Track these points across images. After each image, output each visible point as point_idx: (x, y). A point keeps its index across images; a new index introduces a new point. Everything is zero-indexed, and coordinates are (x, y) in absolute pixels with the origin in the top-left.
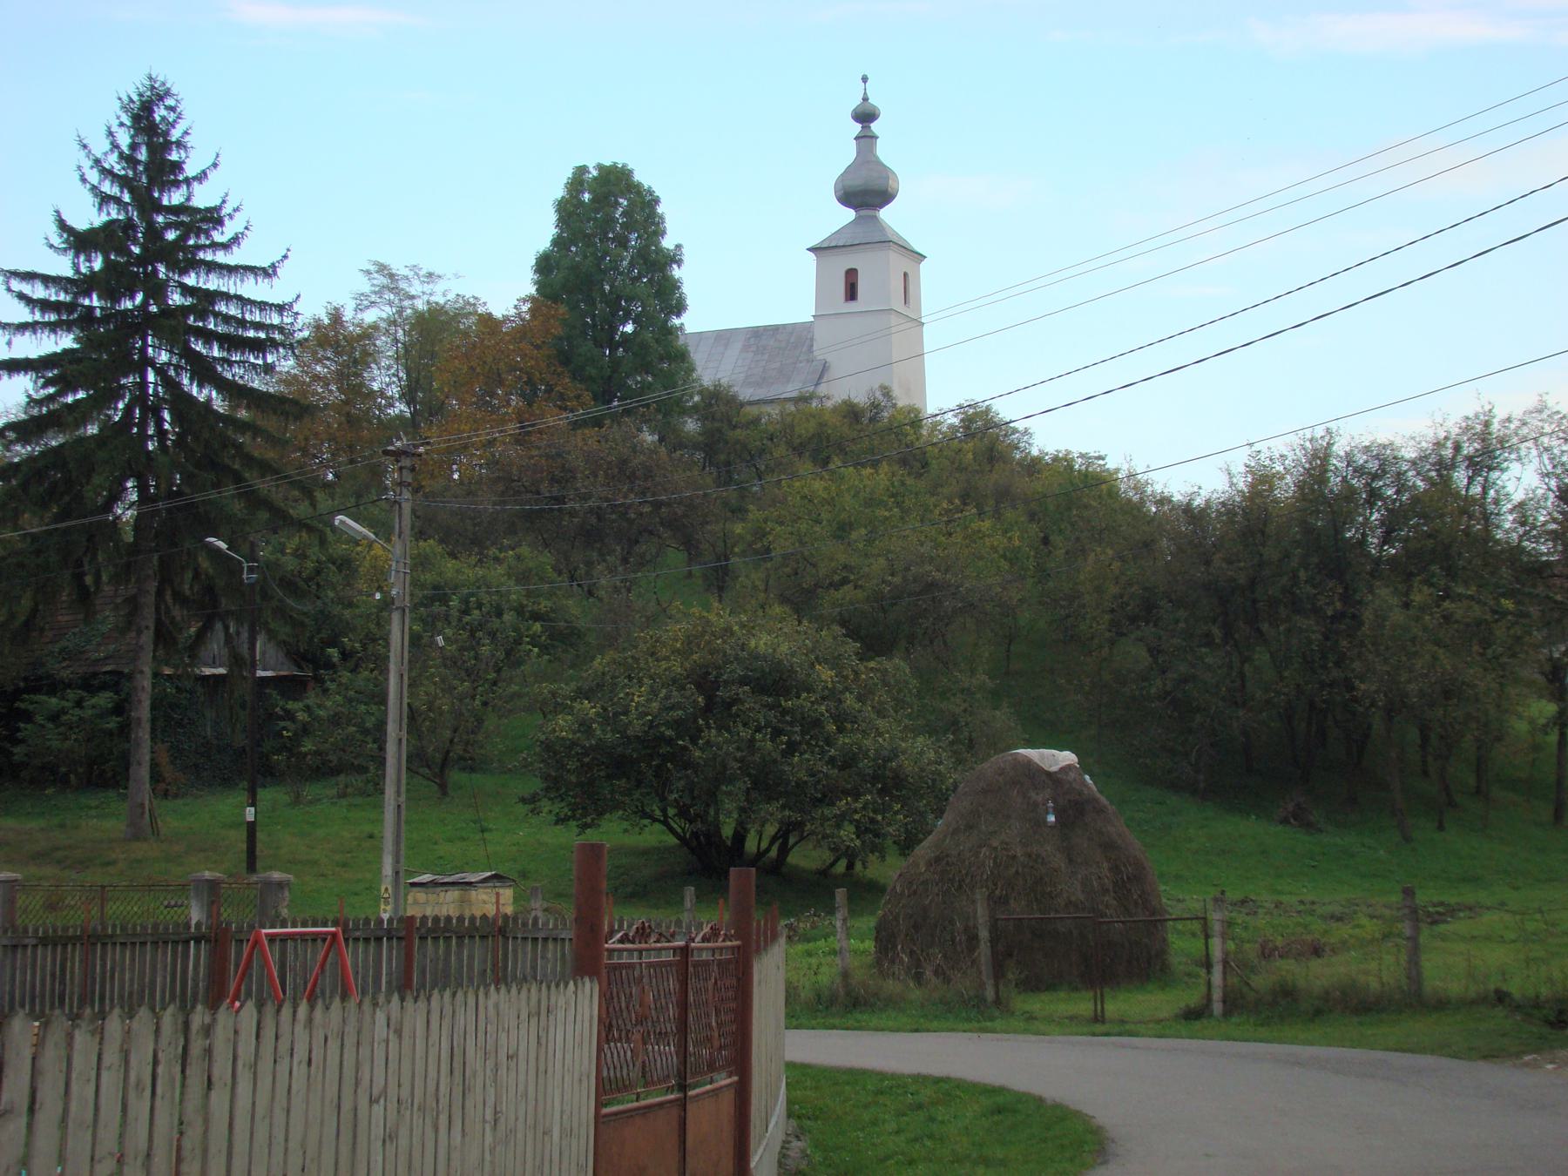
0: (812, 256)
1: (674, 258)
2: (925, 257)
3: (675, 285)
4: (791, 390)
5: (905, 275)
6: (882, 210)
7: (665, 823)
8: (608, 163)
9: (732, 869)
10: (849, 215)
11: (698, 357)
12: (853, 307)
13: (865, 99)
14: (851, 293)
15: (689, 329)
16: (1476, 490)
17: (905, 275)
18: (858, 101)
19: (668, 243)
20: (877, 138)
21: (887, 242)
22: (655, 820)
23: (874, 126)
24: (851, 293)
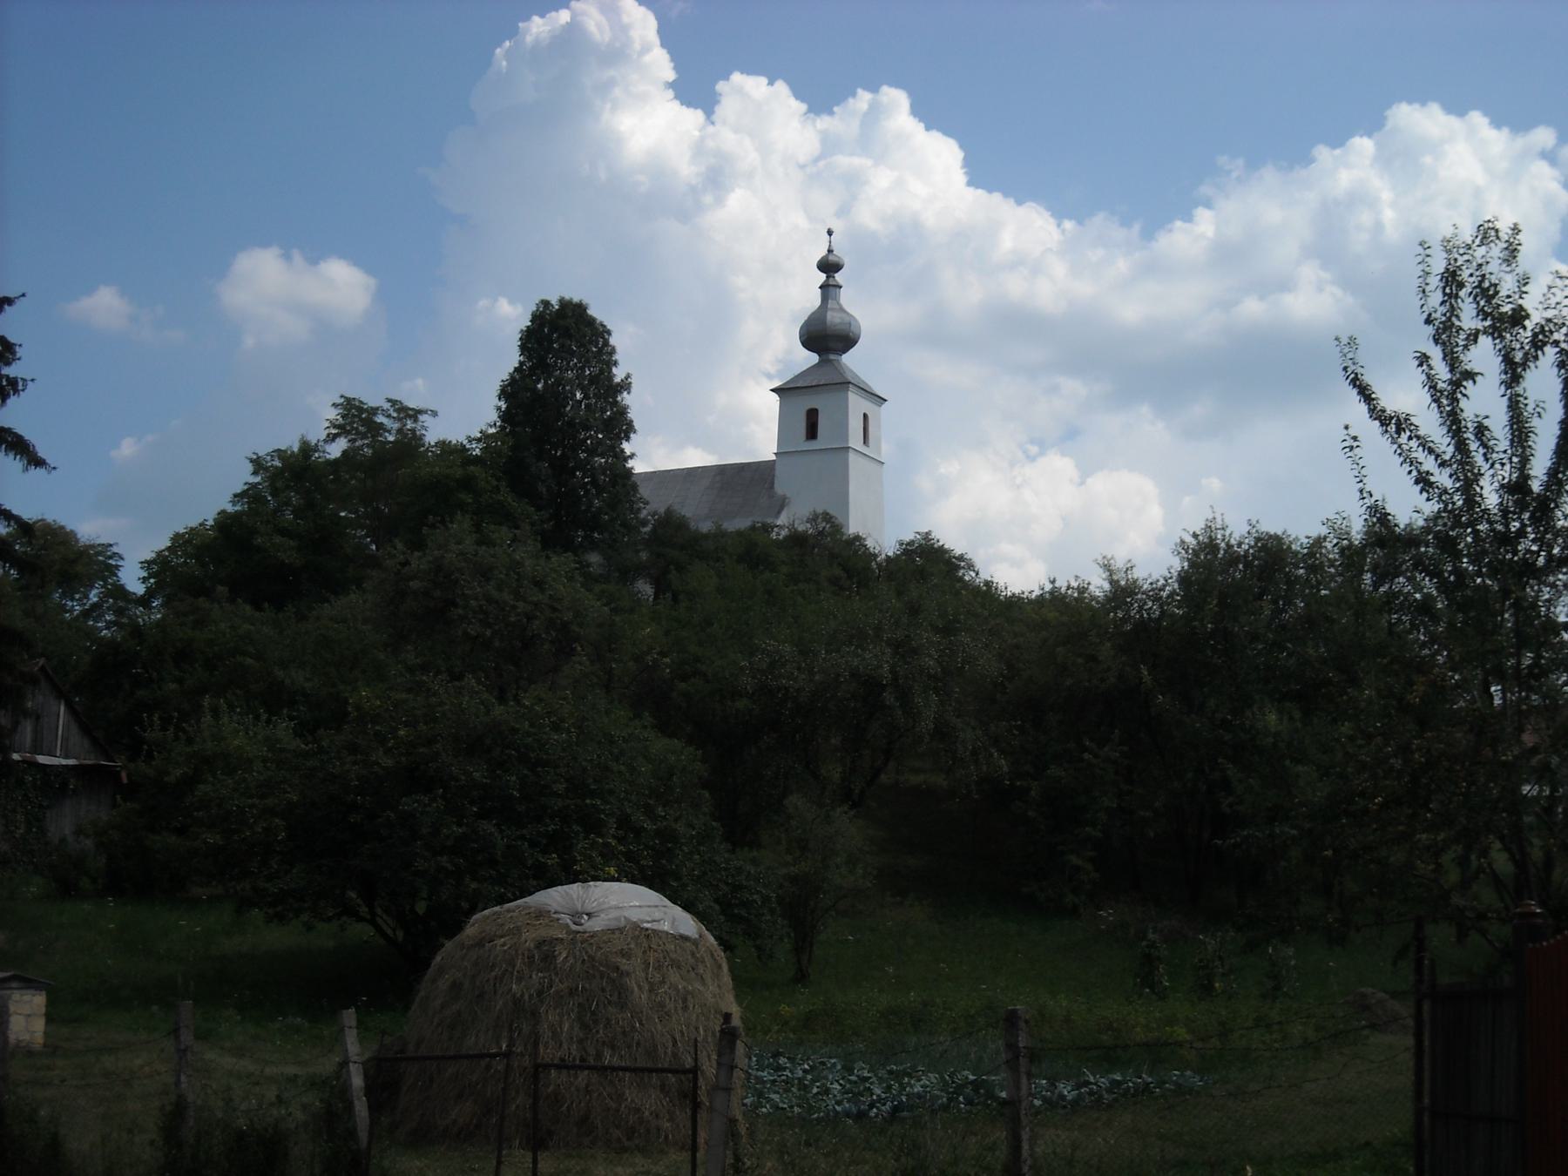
0: (775, 397)
1: (625, 386)
2: (886, 400)
3: (622, 412)
4: (740, 523)
5: (865, 416)
6: (844, 356)
7: (373, 922)
8: (567, 297)
9: (227, 589)
10: (814, 358)
11: (644, 491)
12: (813, 445)
13: (830, 251)
14: (812, 433)
15: (637, 471)
16: (1364, 686)
17: (865, 416)
18: (823, 252)
19: (619, 374)
20: (841, 287)
21: (843, 384)
22: (360, 919)
23: (839, 277)
24: (812, 433)
